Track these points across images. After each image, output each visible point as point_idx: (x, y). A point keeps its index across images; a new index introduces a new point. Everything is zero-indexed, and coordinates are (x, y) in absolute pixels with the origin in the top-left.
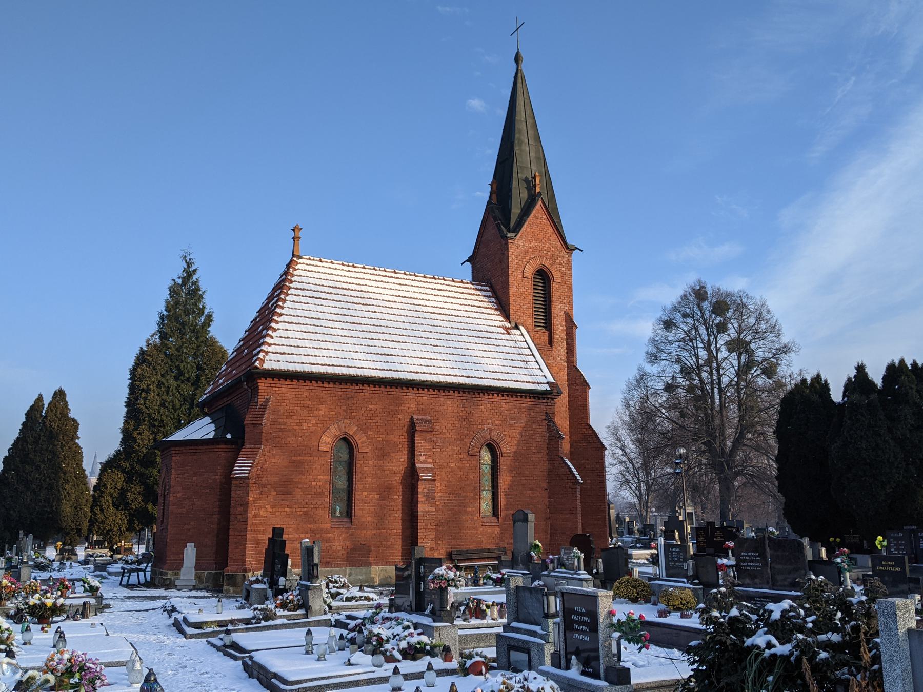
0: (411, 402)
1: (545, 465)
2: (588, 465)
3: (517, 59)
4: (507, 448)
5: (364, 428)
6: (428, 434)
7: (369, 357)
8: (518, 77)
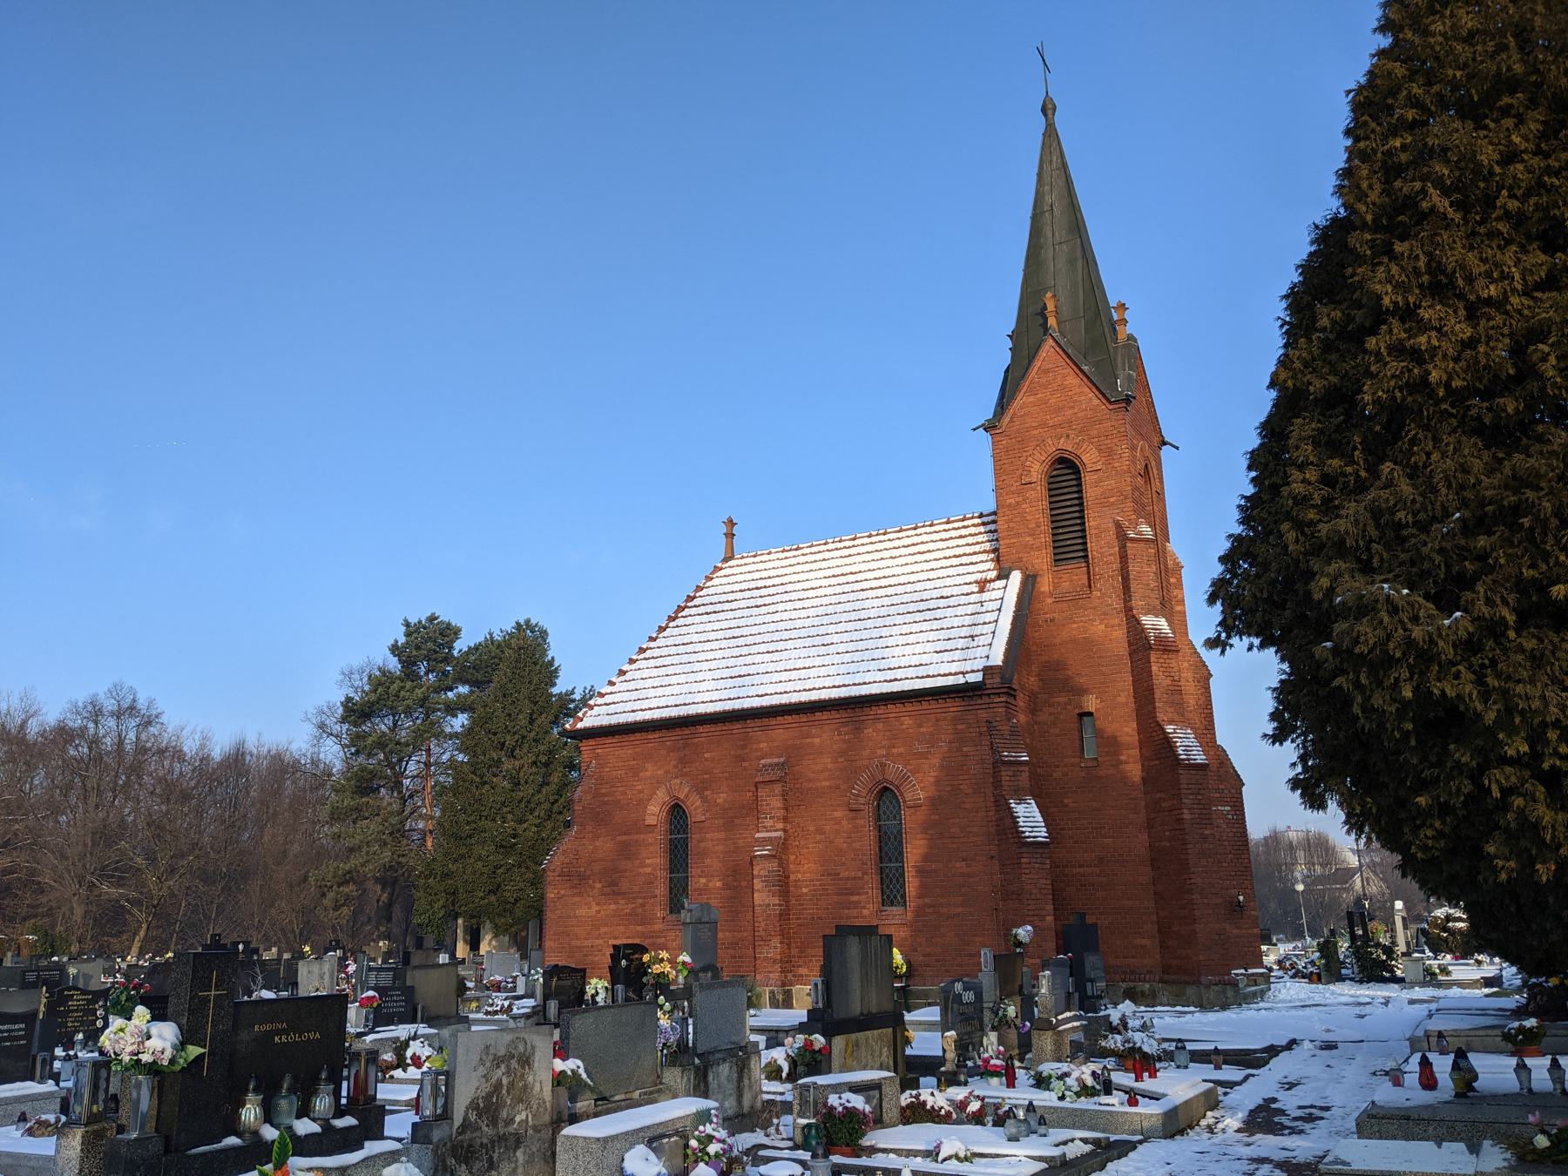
0: (770, 742)
1: (991, 813)
2: (1165, 800)
3: (1048, 109)
4: (918, 791)
5: (700, 788)
6: (775, 786)
7: (721, 684)
8: (1051, 135)
